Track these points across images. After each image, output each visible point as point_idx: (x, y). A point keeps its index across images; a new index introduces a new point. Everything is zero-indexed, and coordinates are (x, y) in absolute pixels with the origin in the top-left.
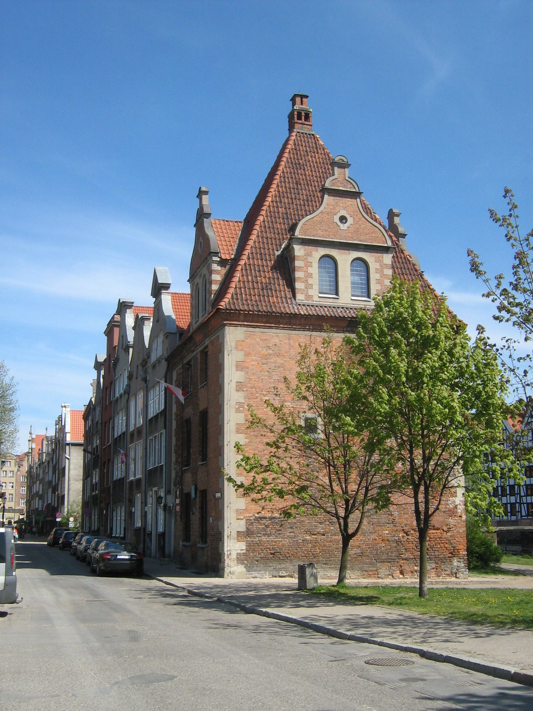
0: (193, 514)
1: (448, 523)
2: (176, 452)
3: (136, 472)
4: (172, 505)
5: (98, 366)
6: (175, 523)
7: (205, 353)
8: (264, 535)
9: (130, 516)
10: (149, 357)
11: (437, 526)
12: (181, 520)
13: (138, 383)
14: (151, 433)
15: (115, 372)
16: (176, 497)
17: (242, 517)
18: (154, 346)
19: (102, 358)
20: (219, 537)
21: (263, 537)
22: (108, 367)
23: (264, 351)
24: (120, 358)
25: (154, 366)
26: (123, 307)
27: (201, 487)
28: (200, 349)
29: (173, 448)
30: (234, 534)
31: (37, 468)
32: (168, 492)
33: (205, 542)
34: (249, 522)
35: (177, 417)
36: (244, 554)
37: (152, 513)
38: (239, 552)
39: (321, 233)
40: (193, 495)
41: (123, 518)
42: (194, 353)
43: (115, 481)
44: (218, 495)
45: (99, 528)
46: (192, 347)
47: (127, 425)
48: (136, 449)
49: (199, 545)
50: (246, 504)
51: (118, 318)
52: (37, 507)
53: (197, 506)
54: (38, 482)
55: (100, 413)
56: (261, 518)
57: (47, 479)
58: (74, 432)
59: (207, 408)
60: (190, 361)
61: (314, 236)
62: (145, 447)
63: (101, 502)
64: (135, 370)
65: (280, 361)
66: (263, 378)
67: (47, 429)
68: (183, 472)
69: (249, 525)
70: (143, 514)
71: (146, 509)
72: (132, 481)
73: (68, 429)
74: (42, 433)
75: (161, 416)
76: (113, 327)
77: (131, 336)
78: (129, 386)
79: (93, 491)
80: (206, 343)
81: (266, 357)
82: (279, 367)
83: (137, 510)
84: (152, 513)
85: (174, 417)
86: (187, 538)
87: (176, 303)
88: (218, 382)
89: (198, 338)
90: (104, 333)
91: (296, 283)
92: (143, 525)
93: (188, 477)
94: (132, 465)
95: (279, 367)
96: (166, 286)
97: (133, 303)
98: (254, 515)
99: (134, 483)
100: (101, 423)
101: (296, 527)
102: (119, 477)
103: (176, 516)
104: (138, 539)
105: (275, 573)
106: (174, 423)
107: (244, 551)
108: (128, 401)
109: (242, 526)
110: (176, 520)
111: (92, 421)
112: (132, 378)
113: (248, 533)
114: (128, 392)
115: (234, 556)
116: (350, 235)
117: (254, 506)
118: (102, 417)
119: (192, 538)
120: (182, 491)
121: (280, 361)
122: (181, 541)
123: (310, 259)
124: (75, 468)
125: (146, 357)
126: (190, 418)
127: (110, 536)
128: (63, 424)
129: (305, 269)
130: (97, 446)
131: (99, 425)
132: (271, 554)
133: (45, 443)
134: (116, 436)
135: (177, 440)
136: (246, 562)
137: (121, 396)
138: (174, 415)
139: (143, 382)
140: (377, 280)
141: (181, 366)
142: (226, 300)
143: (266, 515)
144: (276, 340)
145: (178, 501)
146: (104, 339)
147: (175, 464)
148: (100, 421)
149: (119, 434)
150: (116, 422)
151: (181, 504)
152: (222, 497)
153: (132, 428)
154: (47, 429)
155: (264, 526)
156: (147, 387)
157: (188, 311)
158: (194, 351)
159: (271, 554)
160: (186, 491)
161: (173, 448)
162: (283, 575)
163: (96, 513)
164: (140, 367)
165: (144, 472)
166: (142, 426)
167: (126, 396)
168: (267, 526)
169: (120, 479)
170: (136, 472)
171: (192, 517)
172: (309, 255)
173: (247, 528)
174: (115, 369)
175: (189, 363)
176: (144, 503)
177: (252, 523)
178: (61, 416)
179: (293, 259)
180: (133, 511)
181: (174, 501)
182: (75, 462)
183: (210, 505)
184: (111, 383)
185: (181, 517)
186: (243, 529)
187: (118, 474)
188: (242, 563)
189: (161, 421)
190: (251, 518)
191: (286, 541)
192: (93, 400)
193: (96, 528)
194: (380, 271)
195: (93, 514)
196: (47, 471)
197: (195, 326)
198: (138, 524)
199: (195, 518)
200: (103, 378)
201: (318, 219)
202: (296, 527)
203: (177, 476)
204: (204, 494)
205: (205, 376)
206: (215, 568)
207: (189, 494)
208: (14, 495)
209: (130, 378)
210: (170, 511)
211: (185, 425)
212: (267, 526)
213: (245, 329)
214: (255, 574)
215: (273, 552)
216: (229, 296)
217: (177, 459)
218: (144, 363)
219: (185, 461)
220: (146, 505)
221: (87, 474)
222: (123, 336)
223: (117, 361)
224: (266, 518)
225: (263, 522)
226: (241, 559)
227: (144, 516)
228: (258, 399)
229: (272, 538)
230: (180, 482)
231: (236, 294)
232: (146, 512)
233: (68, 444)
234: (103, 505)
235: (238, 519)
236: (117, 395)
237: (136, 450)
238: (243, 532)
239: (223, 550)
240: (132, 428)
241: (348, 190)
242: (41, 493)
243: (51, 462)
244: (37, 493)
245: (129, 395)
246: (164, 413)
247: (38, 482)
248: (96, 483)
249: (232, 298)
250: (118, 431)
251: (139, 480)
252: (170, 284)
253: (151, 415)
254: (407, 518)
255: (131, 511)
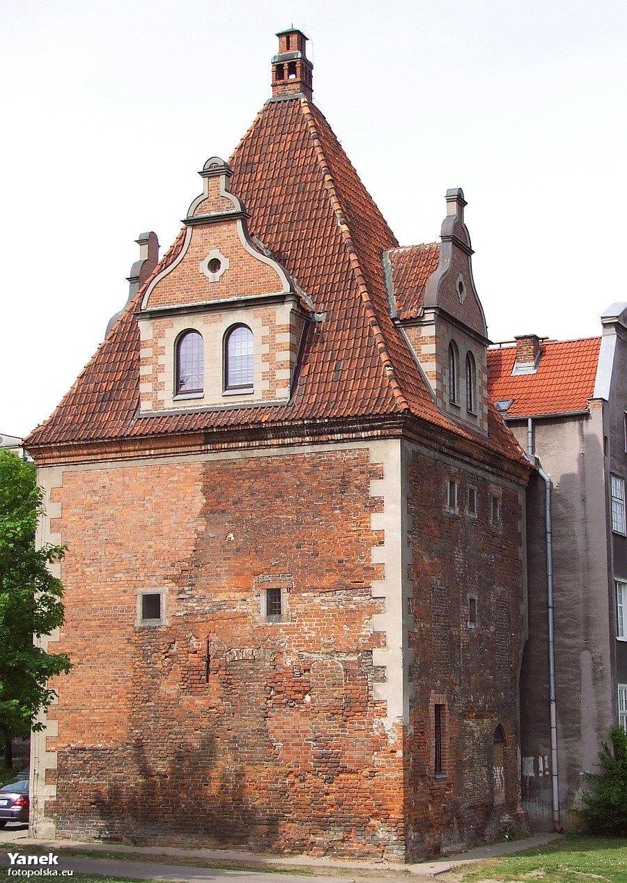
1: (370, 762)
8: (83, 775)
11: (350, 766)
17: (53, 748)
23: (90, 499)
36: (55, 803)
38: (48, 799)
39: (181, 296)
61: (169, 303)
65: (110, 511)
66: (85, 539)
69: (63, 760)
81: (90, 507)
82: (109, 520)
91: (288, 322)
95: (109, 520)
107: (55, 799)
109: (51, 761)
115: (41, 806)
116: (224, 288)
121: (110, 511)
123: (161, 342)
129: (154, 360)
140: (264, 355)
144: (105, 480)
155: (81, 762)
168: (86, 762)
172: (160, 335)
179: (137, 345)
186: (53, 765)
188: (51, 817)
194: (159, 386)
201: (177, 274)
205: (409, 570)
212: (86, 762)
213: (63, 468)
214: (67, 832)
226: (52, 810)
228: (79, 573)
241: (225, 212)
254: (297, 753)
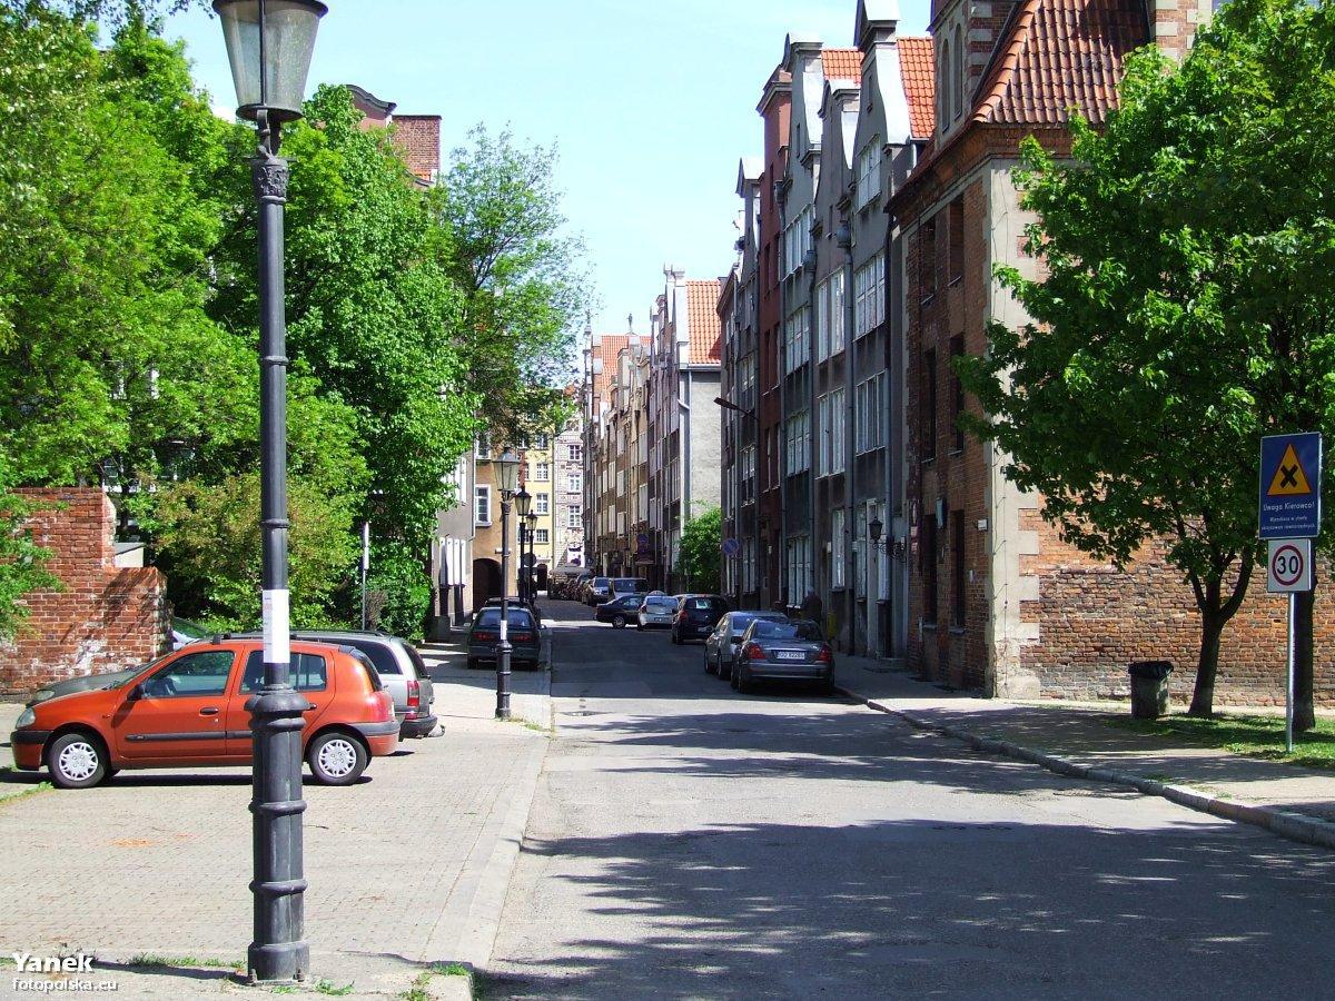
0: (942, 562)
2: (910, 423)
3: (834, 462)
4: (903, 540)
5: (745, 187)
6: (910, 580)
7: (958, 205)
8: (1080, 609)
9: (824, 560)
10: (854, 190)
12: (921, 575)
13: (831, 252)
14: (863, 372)
15: (783, 210)
16: (911, 524)
17: (1030, 571)
18: (865, 170)
19: (756, 169)
20: (984, 614)
21: (1078, 614)
22: (768, 194)
24: (794, 179)
25: (864, 214)
26: (797, 55)
27: (954, 506)
28: (950, 198)
29: (905, 415)
30: (1015, 607)
31: (608, 428)
32: (895, 512)
33: (962, 623)
34: (1048, 583)
35: (911, 343)
37: (864, 559)
40: (940, 523)
41: (808, 565)
42: (940, 205)
43: (792, 478)
44: (982, 524)
45: (758, 589)
46: (934, 190)
47: (813, 348)
48: (831, 405)
49: (952, 629)
50: (1041, 542)
51: (785, 77)
52: (612, 529)
53: (948, 546)
54: (612, 464)
55: (760, 298)
56: (1073, 573)
57: (634, 461)
58: (695, 343)
59: (963, 333)
60: (933, 219)
62: (849, 404)
63: (762, 525)
64: (826, 218)
67: (630, 319)
68: (923, 469)
70: (850, 557)
71: (855, 546)
72: (826, 478)
73: (682, 333)
74: (620, 329)
75: (880, 335)
76: (777, 98)
77: (815, 130)
78: (814, 253)
79: (744, 499)
80: (961, 188)
83: (836, 547)
84: (864, 559)
85: (905, 343)
86: (931, 616)
87: (911, 67)
88: (981, 278)
89: (945, 174)
90: (758, 108)
92: (850, 584)
93: (932, 477)
94: (829, 439)
96: (887, 27)
97: (819, 45)
98: (1058, 567)
99: (830, 485)
100: (758, 334)
101: (1152, 594)
102: (798, 469)
103: (911, 566)
104: (826, 617)
105: (1103, 690)
106: (906, 354)
107: (1037, 643)
108: (813, 288)
109: (1031, 590)
110: (911, 574)
111: (738, 324)
112: (821, 233)
113: (1041, 607)
114: (811, 266)
115: (1015, 651)
117: (1057, 548)
118: (758, 319)
119: (941, 614)
120: (921, 509)
122: (921, 619)
124: (703, 435)
125: (848, 191)
126: (934, 349)
127: (782, 607)
128: (670, 320)
130: (749, 389)
131: (753, 339)
132: (1096, 649)
133: (627, 361)
134: (789, 371)
135: (911, 393)
136: (1039, 665)
137: (798, 272)
138: (904, 337)
139: (843, 250)
141: (915, 228)
142: (994, 101)
143: (1083, 567)
145: (914, 531)
146: (759, 123)
147: (908, 449)
148: (754, 329)
149: (797, 366)
150: (788, 336)
151: (920, 537)
152: (989, 529)
153: (822, 356)
154: (630, 319)
156: (851, 264)
157: (929, 93)
158: (937, 200)
159: (1096, 649)
160: (928, 512)
161: (905, 415)
162: (1120, 693)
163: (752, 555)
164: (837, 213)
165: (849, 462)
166: (843, 353)
167: (809, 277)
168: (1086, 591)
169: (800, 475)
170: (834, 462)
171: (940, 568)
173: (1043, 594)
174: (783, 203)
175: (931, 223)
176: (851, 533)
177: (1054, 584)
178: (666, 295)
180: (829, 549)
181: (907, 532)
182: (703, 418)
183: (970, 544)
184: (777, 237)
185: (920, 567)
187: (797, 462)
189: (880, 345)
190: (1052, 574)
191: (1127, 624)
192: (738, 272)
193: (753, 588)
195: (745, 553)
196: (634, 438)
197: (944, 139)
198: (839, 576)
199: (945, 570)
200: (759, 222)
202: (1152, 594)
203: (912, 475)
204: (960, 516)
206: (978, 681)
207: (933, 518)
208: (550, 497)
209: (816, 232)
210: (900, 554)
211: (926, 360)
215: (1099, 644)
216: (1001, 90)
217: (912, 438)
218: (846, 203)
219: (926, 448)
220: (854, 538)
221: (730, 458)
222: (799, 128)
223: (786, 186)
224: (1083, 573)
225: (1077, 581)
226: (1033, 658)
227: (851, 561)
229: (1096, 616)
230: (917, 492)
231: (1019, 85)
232: (854, 554)
233: (684, 373)
234: (765, 533)
235: (1022, 575)
236: (790, 271)
237: (833, 411)
238: (1035, 602)
239: (992, 640)
240: (822, 356)
242: (620, 493)
243: (643, 415)
244: (612, 492)
245: (814, 274)
246: (885, 329)
247: (612, 464)
248: (750, 480)
249: (1009, 95)
250: (795, 357)
251: (840, 479)
252: (895, 22)
253: (858, 334)
255: (825, 550)
